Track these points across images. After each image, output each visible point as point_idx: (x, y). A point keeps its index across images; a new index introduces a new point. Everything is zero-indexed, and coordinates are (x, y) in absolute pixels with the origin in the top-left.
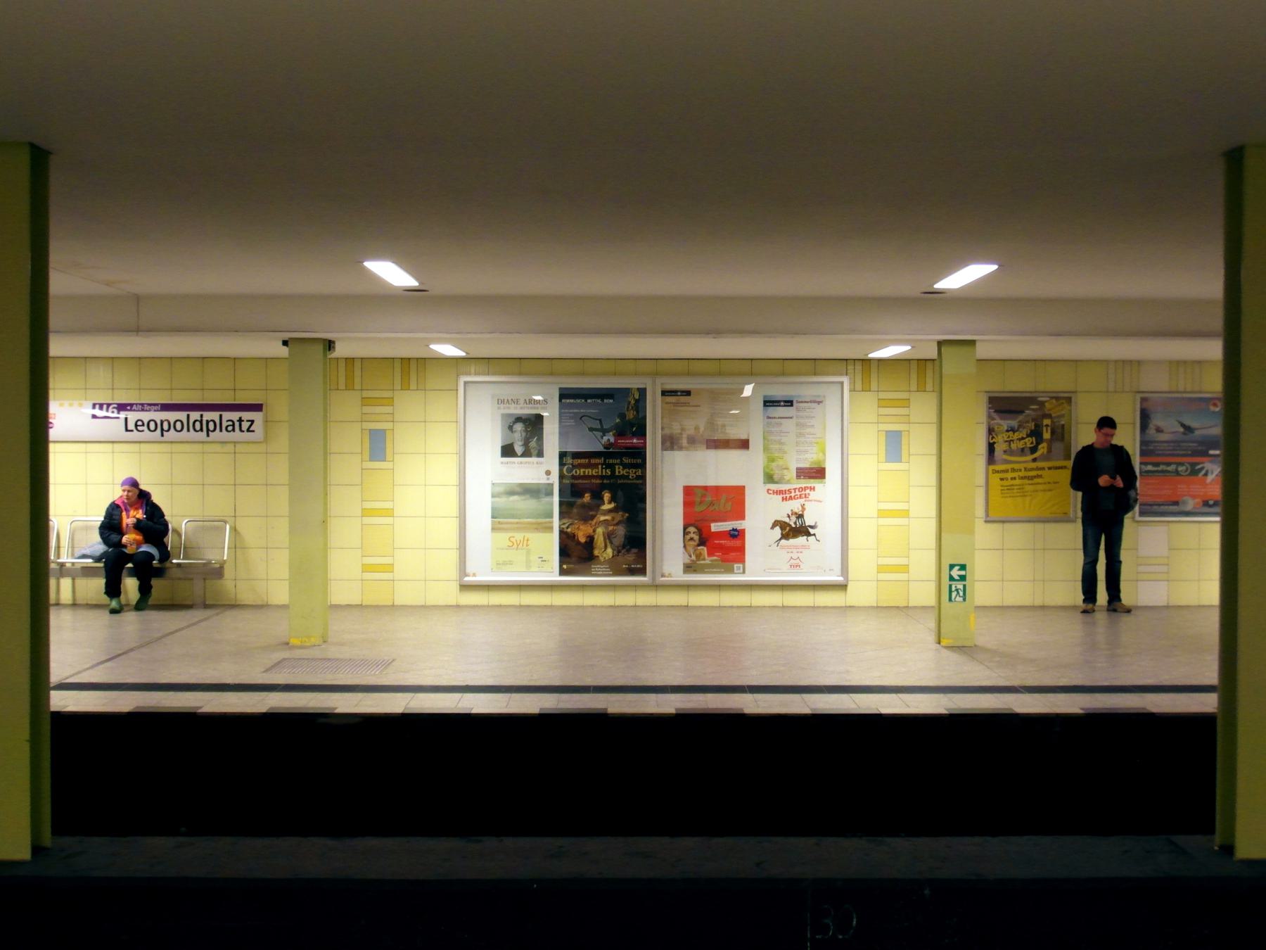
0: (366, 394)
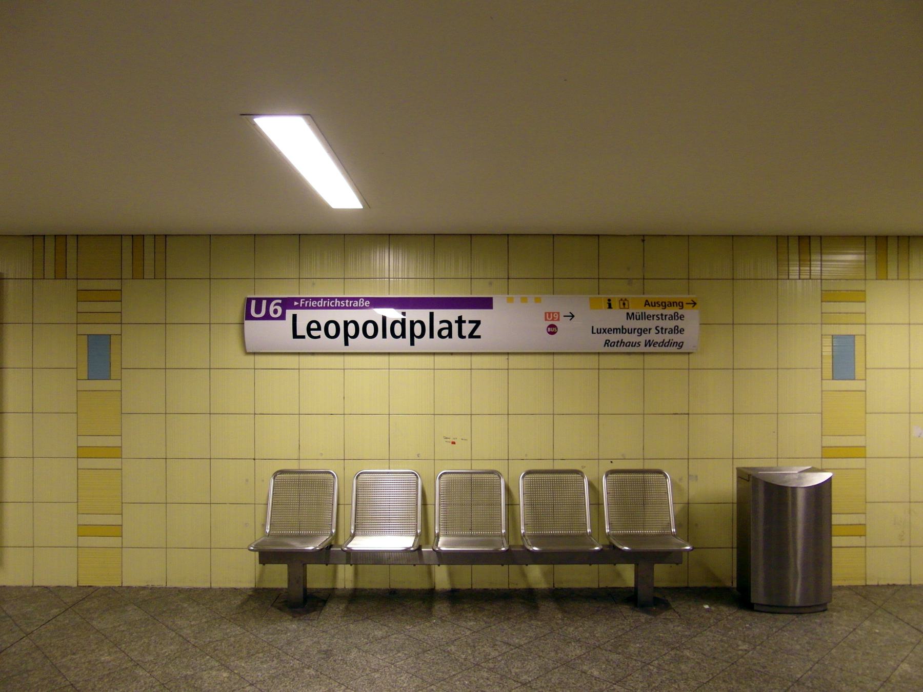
0: (83, 285)
